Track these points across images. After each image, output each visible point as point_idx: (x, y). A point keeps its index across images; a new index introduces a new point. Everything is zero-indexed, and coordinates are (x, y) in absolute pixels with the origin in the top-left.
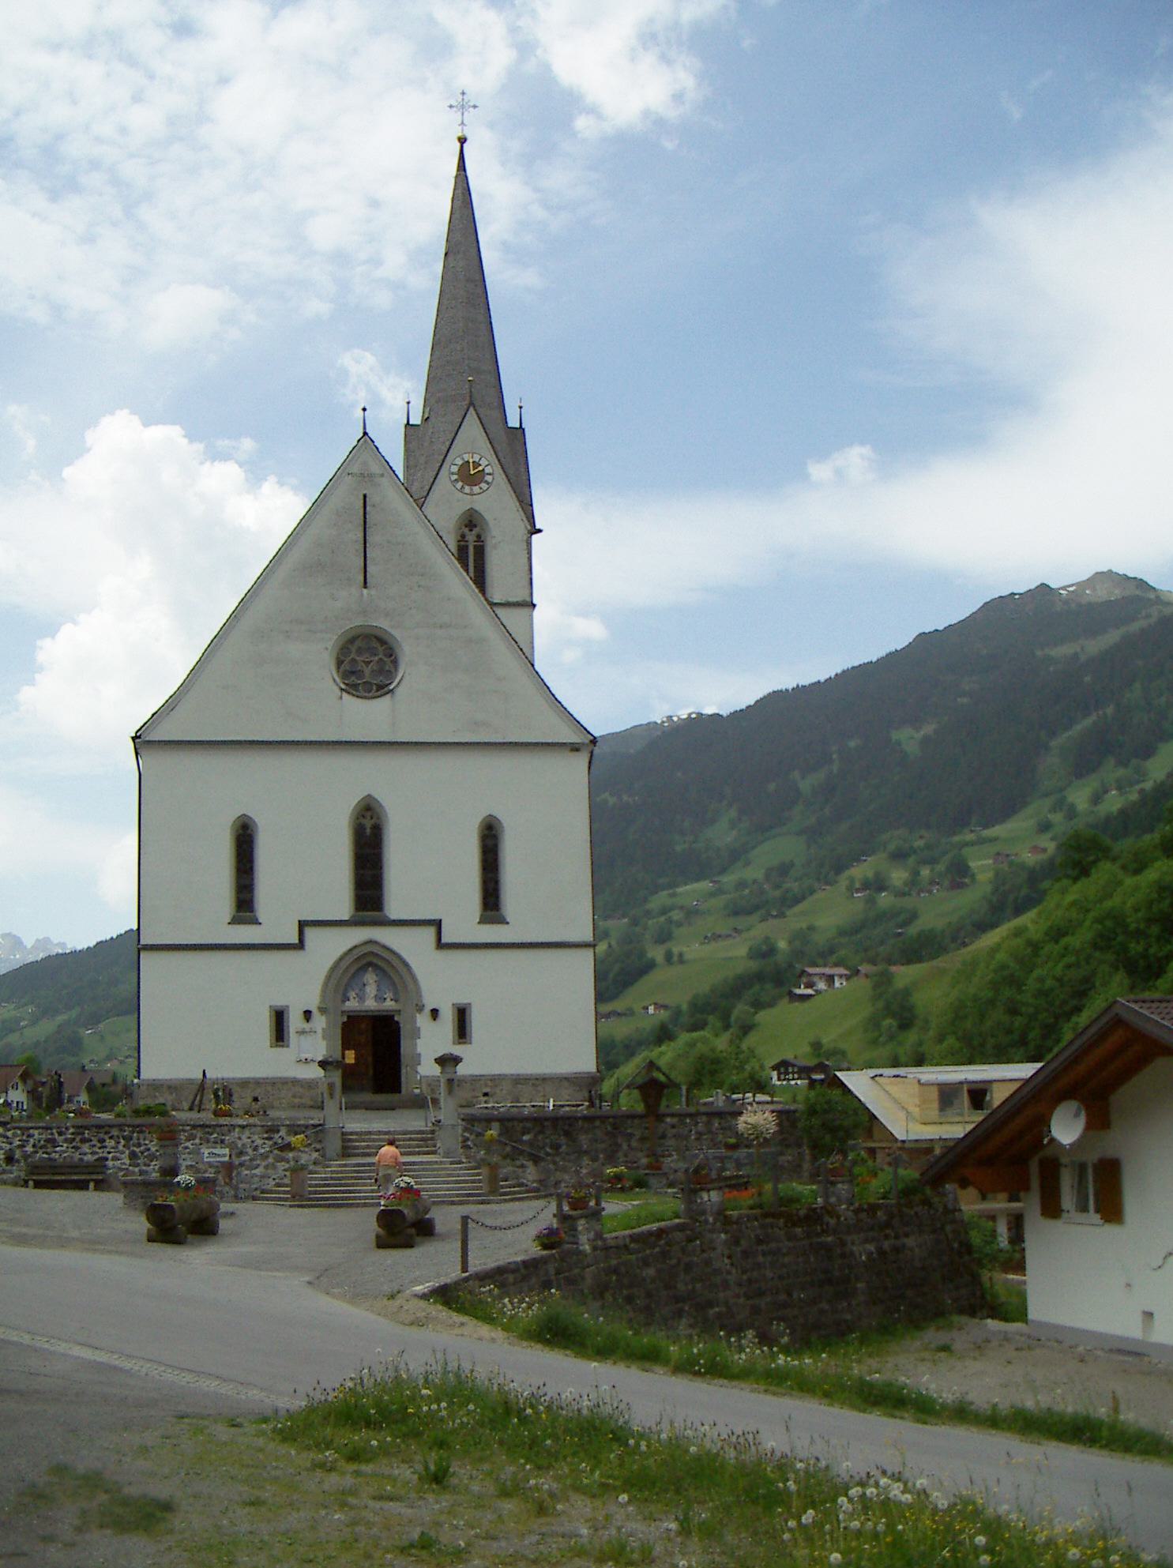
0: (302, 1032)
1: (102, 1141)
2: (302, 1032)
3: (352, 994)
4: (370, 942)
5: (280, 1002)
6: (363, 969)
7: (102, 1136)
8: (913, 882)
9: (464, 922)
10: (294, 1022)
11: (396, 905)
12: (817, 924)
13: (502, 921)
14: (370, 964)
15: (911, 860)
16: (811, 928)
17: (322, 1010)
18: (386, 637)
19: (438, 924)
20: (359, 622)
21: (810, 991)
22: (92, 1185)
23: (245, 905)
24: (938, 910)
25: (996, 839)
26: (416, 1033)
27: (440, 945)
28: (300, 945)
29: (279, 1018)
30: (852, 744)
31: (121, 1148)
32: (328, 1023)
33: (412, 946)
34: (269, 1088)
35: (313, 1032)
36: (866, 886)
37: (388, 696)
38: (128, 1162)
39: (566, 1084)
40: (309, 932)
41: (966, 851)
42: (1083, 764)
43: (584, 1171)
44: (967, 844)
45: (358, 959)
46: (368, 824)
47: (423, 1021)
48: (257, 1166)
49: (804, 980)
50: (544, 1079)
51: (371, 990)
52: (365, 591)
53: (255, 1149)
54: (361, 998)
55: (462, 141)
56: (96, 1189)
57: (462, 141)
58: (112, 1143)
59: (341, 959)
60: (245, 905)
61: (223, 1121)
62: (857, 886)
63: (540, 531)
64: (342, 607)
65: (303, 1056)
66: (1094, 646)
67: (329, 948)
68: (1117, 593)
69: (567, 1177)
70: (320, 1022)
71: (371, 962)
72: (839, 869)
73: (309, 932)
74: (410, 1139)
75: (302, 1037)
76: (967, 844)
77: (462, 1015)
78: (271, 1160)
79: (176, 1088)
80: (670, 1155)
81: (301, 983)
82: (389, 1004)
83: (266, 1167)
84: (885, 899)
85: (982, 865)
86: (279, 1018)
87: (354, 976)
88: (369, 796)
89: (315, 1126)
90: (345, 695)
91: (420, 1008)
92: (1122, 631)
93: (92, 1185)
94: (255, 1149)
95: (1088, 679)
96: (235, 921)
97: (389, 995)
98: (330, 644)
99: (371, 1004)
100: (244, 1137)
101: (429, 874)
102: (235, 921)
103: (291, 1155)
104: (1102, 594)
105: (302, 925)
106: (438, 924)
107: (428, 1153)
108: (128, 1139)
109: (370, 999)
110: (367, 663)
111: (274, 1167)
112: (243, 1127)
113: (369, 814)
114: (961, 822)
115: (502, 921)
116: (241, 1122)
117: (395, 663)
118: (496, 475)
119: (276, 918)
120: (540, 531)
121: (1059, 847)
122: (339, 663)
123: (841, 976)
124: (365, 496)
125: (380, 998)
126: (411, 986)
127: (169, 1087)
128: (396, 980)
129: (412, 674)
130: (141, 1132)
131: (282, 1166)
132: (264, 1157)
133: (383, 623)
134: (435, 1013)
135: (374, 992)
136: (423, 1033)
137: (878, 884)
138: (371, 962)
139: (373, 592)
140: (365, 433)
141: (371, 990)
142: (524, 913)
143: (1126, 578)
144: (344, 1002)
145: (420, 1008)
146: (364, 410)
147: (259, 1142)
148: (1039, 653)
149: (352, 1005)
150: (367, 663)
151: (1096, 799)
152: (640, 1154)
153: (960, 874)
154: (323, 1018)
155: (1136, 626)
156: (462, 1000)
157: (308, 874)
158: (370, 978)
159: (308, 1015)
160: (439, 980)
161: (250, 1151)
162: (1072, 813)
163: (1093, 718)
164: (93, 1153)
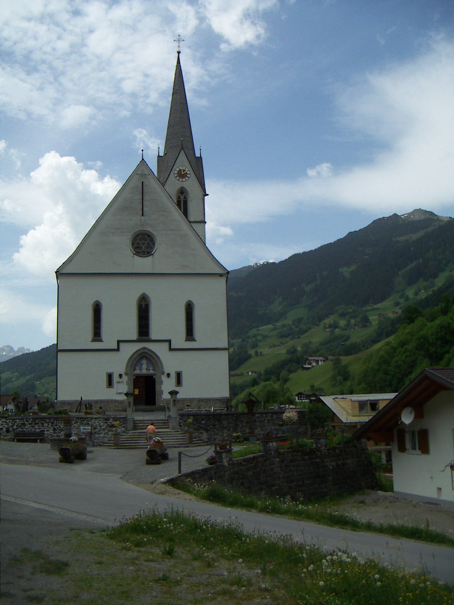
0: (118, 382)
1: (42, 424)
2: (118, 382)
3: (137, 368)
4: (144, 348)
5: (110, 371)
6: (142, 358)
7: (42, 422)
8: (348, 325)
9: (179, 341)
10: (116, 378)
11: (154, 334)
13: (194, 340)
14: (144, 356)
15: (347, 317)
16: (310, 342)
17: (126, 374)
19: (169, 341)
20: (140, 229)
21: (310, 366)
22: (39, 441)
23: (97, 335)
24: (358, 335)
26: (161, 383)
27: (171, 349)
30: (325, 273)
31: (50, 426)
32: (128, 379)
33: (160, 350)
34: (106, 404)
36: (330, 326)
37: (151, 256)
38: (52, 432)
39: (218, 401)
40: (122, 345)
41: (368, 313)
42: (411, 280)
43: (225, 435)
44: (368, 311)
47: (164, 378)
51: (144, 366)
52: (143, 217)
53: (101, 427)
54: (141, 369)
55: (179, 53)
56: (40, 442)
57: (179, 53)
58: (47, 425)
59: (133, 355)
60: (97, 335)
61: (88, 416)
63: (208, 195)
64: (134, 223)
65: (119, 391)
66: (415, 237)
67: (128, 350)
68: (423, 217)
70: (125, 378)
71: (144, 356)
72: (320, 320)
73: (122, 345)
75: (119, 384)
77: (179, 375)
78: (106, 431)
80: (258, 429)
81: (118, 363)
82: (151, 372)
83: (105, 434)
84: (337, 331)
85: (374, 318)
86: (110, 377)
89: (123, 418)
90: (135, 256)
91: (163, 373)
93: (39, 441)
94: (101, 427)
97: (151, 368)
98: (129, 237)
99: (144, 372)
100: (96, 422)
101: (166, 322)
102: (94, 340)
103: (114, 429)
104: (417, 217)
105: (119, 342)
108: (52, 423)
109: (144, 370)
110: (143, 244)
111: (108, 434)
112: (96, 418)
113: (144, 300)
115: (194, 340)
116: (95, 416)
119: (109, 340)
120: (208, 195)
122: (133, 244)
123: (321, 360)
124: (143, 182)
125: (148, 369)
127: (68, 403)
129: (160, 248)
130: (57, 420)
131: (111, 433)
132: (104, 430)
133: (149, 229)
134: (168, 375)
136: (164, 383)
137: (335, 326)
138: (144, 356)
139: (146, 218)
140: (143, 159)
141: (144, 366)
142: (202, 338)
143: (426, 211)
144: (134, 371)
145: (163, 373)
147: (102, 424)
148: (394, 239)
149: (137, 372)
150: (143, 244)
151: (416, 294)
153: (365, 322)
155: (430, 229)
156: (179, 370)
157: (121, 323)
158: (144, 362)
159: (121, 376)
160: (170, 362)
161: (98, 427)
162: (407, 299)
164: (39, 429)
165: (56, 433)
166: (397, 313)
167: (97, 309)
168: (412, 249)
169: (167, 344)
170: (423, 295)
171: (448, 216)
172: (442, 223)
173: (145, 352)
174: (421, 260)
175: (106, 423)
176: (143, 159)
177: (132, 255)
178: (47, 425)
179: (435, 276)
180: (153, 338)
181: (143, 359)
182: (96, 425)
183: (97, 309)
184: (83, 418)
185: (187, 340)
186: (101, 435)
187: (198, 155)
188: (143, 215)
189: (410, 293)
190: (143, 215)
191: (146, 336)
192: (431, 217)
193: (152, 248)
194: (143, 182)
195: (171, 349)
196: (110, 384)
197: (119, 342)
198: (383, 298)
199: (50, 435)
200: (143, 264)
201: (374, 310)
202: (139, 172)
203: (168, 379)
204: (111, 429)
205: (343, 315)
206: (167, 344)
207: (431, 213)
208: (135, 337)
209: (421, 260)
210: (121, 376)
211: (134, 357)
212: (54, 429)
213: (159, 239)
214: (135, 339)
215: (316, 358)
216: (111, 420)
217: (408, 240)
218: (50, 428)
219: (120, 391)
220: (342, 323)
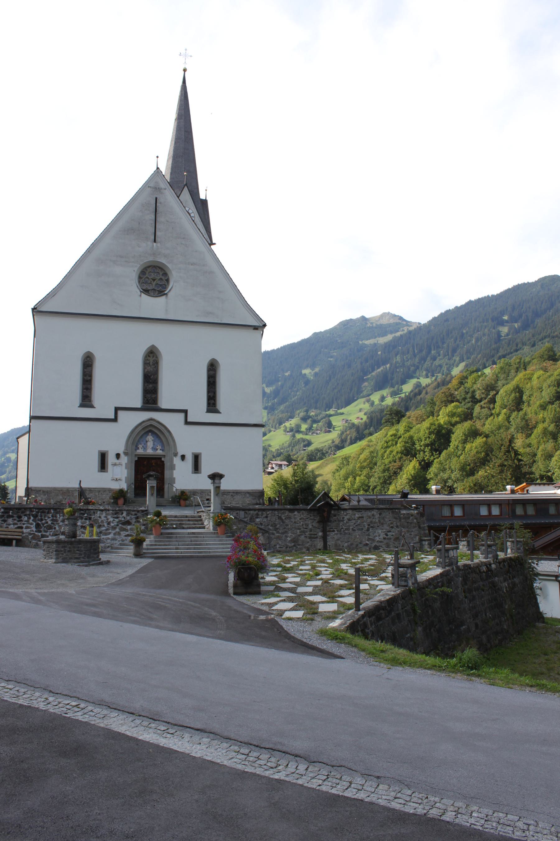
0: (115, 465)
1: (20, 517)
2: (115, 465)
3: (140, 446)
4: (151, 419)
5: (103, 449)
6: (147, 433)
7: (20, 514)
8: (310, 429)
9: (198, 412)
10: (111, 459)
11: (164, 402)
12: (272, 444)
13: (217, 412)
14: (150, 431)
15: (309, 421)
16: (270, 446)
17: (126, 454)
18: (164, 268)
19: (185, 412)
20: (151, 259)
21: (272, 471)
22: (14, 542)
23: (86, 400)
24: (321, 440)
25: (343, 414)
26: (173, 467)
27: (187, 423)
28: (115, 420)
29: (103, 457)
30: (287, 374)
31: (31, 521)
32: (128, 460)
33: (172, 422)
34: (97, 494)
35: (120, 464)
36: (291, 430)
37: (164, 297)
38: (34, 529)
39: (248, 495)
40: (120, 413)
41: (331, 418)
42: (379, 386)
43: (289, 539)
44: (331, 415)
45: (143, 429)
46: (151, 360)
47: (177, 461)
48: (110, 533)
49: (270, 466)
50: (237, 493)
51: (150, 444)
52: (155, 244)
53: (109, 523)
54: (145, 448)
55: (185, 70)
56: (17, 545)
57: (185, 70)
58: (26, 518)
59: (136, 427)
60: (86, 400)
61: (90, 507)
62: (288, 430)
63: (215, 244)
64: (143, 250)
65: (116, 477)
66: (382, 340)
67: (130, 421)
68: (392, 321)
69: (280, 542)
70: (124, 460)
71: (151, 429)
72: (280, 424)
73: (120, 413)
74: (189, 521)
75: (115, 467)
76: (331, 415)
77: (197, 458)
78: (117, 530)
79: (47, 492)
80: (334, 531)
81: (115, 438)
82: (159, 452)
83: (115, 534)
84: (299, 436)
85: (337, 422)
86: (103, 457)
87: (141, 437)
88: (153, 345)
89: (143, 511)
90: (142, 294)
91: (176, 455)
92: (393, 335)
93: (14, 542)
94: (109, 523)
95: (379, 353)
96: (82, 406)
97: (159, 447)
98: (136, 269)
99: (150, 451)
100: (103, 517)
101: (181, 387)
102: (82, 406)
103: (129, 527)
104: (385, 321)
105: (117, 409)
106: (185, 412)
107: (200, 528)
108: (35, 516)
109: (150, 448)
110: (154, 280)
111: (119, 534)
112: (102, 510)
113: (151, 355)
114: (329, 407)
115: (217, 412)
116: (101, 508)
117: (168, 281)
118: (196, 216)
119: (103, 406)
120: (215, 244)
121: (368, 417)
122: (140, 278)
123: (285, 465)
124: (156, 199)
125: (154, 449)
126: (171, 443)
127: (44, 492)
128: (163, 439)
129: (176, 287)
130: (42, 512)
131: (123, 533)
132: (114, 528)
133: (164, 261)
134: (183, 457)
135: (152, 446)
136: (177, 467)
137: (297, 430)
138: (151, 429)
139: (159, 245)
140: (158, 168)
141: (150, 444)
142: (228, 409)
143: (395, 316)
144: (136, 450)
145: (176, 455)
146: (157, 157)
147: (111, 519)
148: (360, 342)
149: (140, 451)
150: (154, 280)
151: (383, 399)
152: (318, 530)
153: (330, 426)
154: (126, 458)
155: (398, 334)
156: (197, 451)
157: (119, 384)
158: (150, 438)
159: (118, 456)
160: (186, 441)
161: (106, 525)
162: (372, 404)
163: (382, 368)
164: (14, 524)
165: (41, 532)
166: (362, 419)
167: (88, 363)
168: (379, 353)
169: (182, 415)
170: (389, 401)
171: (417, 322)
172: (411, 329)
173: (151, 425)
174: (388, 366)
175: (117, 518)
176: (158, 168)
177: (139, 293)
178: (26, 518)
179: (404, 382)
180: (163, 407)
181: (148, 435)
182: (102, 521)
183: (88, 363)
184: (82, 510)
185: (208, 411)
186: (110, 536)
187: (202, 197)
188: (155, 241)
189: (375, 398)
190: (155, 241)
191: (153, 404)
192: (400, 321)
193: (165, 287)
194: (156, 199)
195: (187, 423)
196: (103, 466)
197: (117, 409)
198: (348, 403)
199: (30, 534)
200: (153, 306)
201: (337, 414)
202: (152, 185)
203: (182, 462)
204: (124, 527)
205: (304, 419)
206: (182, 415)
207: (401, 318)
208: (138, 403)
209: (388, 366)
210: (118, 456)
211: (140, 428)
212: (38, 526)
213: (174, 276)
214: (139, 406)
215: (280, 463)
216: (125, 514)
217: (375, 344)
218: (32, 524)
219: (119, 477)
220: (304, 427)
